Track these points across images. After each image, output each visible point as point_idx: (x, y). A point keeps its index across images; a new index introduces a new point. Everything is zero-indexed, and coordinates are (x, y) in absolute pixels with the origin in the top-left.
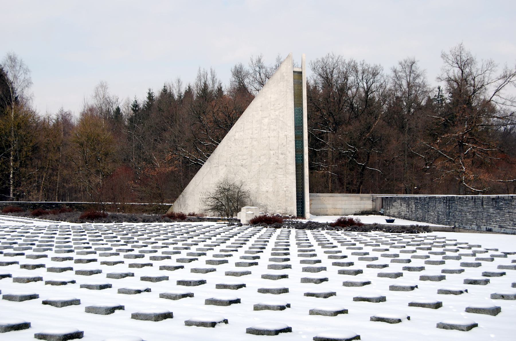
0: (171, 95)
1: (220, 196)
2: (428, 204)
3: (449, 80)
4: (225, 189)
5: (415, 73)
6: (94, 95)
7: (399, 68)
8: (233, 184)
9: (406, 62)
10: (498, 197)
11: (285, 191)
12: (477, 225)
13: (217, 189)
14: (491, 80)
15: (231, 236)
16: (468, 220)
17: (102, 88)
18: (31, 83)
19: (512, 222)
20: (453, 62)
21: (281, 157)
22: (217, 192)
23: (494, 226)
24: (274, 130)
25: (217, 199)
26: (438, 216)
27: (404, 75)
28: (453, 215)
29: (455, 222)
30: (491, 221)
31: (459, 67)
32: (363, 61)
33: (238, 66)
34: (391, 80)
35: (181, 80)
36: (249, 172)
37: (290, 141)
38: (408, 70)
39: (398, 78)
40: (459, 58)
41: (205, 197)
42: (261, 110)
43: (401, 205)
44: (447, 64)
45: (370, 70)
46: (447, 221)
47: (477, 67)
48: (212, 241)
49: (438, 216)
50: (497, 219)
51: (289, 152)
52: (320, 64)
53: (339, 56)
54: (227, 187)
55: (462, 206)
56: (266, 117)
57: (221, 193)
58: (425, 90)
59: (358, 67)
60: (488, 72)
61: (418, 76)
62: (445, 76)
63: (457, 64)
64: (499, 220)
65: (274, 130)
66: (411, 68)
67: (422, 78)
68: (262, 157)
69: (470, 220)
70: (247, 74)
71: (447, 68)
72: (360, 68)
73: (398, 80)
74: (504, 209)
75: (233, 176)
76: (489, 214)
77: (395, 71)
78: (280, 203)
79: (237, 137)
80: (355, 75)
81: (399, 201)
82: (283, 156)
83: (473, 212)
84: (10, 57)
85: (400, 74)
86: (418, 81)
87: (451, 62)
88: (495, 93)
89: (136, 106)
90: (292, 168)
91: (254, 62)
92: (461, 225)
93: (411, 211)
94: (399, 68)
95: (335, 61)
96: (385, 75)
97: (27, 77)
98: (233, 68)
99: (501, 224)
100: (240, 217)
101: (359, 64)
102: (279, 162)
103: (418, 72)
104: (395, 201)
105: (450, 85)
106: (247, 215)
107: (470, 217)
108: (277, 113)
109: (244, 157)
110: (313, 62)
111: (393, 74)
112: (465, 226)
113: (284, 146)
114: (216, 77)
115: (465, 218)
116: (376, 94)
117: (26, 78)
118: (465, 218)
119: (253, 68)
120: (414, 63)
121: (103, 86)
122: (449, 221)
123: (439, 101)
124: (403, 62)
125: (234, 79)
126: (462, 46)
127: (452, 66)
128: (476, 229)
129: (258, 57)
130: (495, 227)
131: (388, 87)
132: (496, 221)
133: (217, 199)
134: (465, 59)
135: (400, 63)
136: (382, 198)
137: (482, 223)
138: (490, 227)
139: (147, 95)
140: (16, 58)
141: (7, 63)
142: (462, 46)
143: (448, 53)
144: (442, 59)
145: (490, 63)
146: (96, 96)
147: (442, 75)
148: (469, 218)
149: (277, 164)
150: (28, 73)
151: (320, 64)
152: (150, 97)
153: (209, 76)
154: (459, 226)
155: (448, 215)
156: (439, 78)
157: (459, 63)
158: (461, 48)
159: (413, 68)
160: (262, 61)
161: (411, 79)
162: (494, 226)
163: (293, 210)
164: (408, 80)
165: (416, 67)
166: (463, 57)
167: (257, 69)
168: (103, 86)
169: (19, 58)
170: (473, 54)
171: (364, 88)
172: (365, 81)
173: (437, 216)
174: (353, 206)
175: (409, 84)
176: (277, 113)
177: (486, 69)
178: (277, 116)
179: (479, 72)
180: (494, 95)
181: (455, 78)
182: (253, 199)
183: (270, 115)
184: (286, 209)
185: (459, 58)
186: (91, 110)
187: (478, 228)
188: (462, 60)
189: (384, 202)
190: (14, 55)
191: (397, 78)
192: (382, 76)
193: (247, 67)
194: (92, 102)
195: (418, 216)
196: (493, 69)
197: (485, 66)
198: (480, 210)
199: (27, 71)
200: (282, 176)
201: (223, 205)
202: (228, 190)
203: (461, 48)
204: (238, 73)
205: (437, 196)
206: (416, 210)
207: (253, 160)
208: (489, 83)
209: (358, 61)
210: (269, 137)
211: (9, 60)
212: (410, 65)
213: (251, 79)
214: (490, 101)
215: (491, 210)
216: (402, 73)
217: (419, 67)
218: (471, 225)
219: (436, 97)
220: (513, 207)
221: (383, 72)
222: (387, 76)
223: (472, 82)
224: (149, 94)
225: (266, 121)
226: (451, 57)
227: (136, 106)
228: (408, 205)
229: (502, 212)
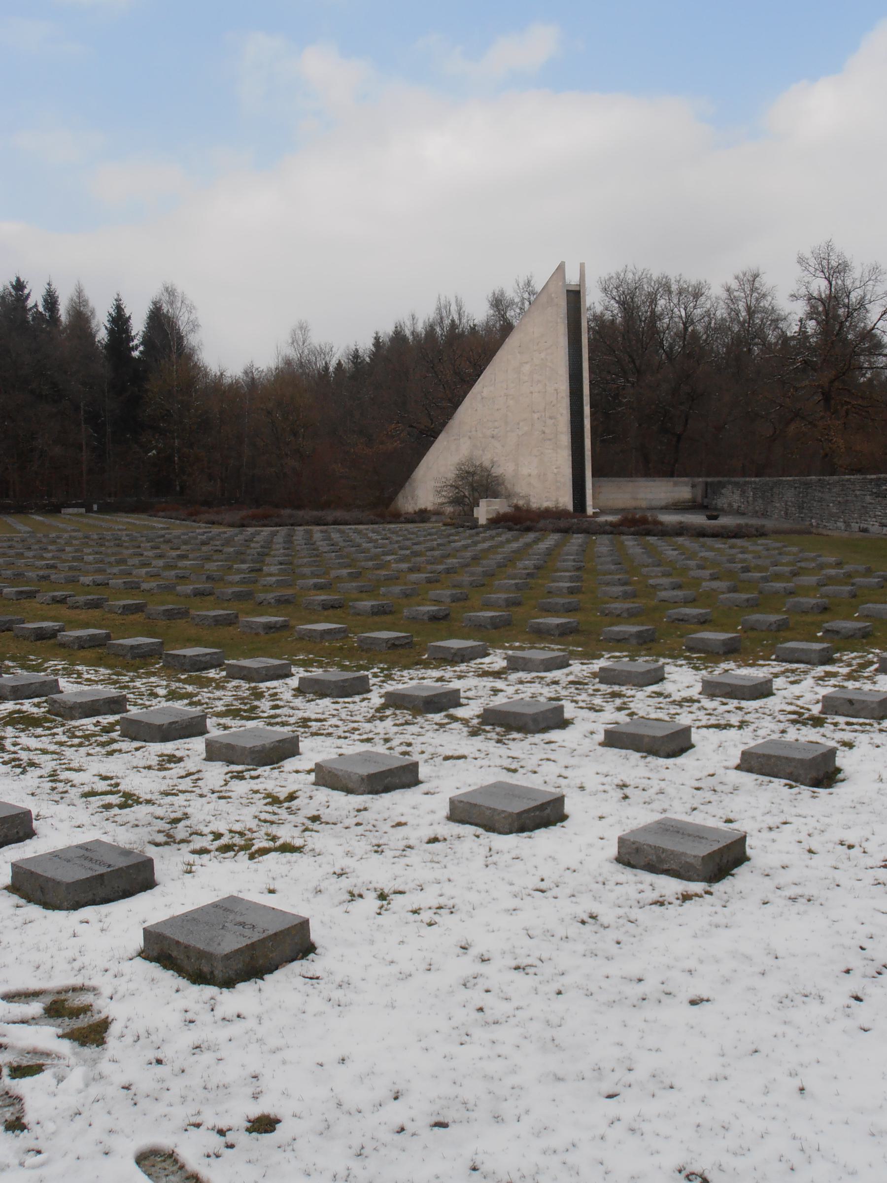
0: (404, 338)
1: (460, 483)
2: (771, 489)
3: (810, 298)
4: (468, 472)
5: (759, 291)
6: (290, 341)
7: (734, 285)
8: (481, 465)
9: (744, 275)
10: (879, 479)
11: (556, 474)
12: (845, 522)
13: (457, 472)
14: (875, 296)
17: (301, 331)
18: (198, 326)
20: (816, 269)
21: (550, 422)
22: (458, 476)
24: (539, 381)
25: (457, 488)
26: (787, 509)
27: (742, 295)
28: (810, 507)
29: (812, 518)
30: (867, 515)
31: (826, 278)
32: (680, 275)
33: (496, 292)
34: (722, 303)
35: (417, 316)
36: (503, 446)
37: (562, 397)
38: (747, 288)
39: (733, 300)
40: (825, 263)
41: (438, 485)
42: (519, 353)
44: (806, 272)
45: (690, 289)
46: (799, 517)
47: (854, 276)
50: (877, 513)
51: (562, 414)
52: (613, 281)
53: (644, 270)
54: (471, 470)
55: (823, 492)
56: (526, 363)
57: (463, 478)
58: (774, 317)
59: (673, 286)
60: (871, 282)
61: (764, 296)
62: (803, 291)
63: (823, 271)
64: (880, 513)
65: (539, 381)
66: (753, 284)
67: (769, 298)
68: (521, 424)
70: (512, 303)
71: (806, 279)
72: (674, 287)
73: (734, 304)
75: (481, 452)
76: (865, 505)
77: (728, 290)
78: (548, 492)
79: (485, 394)
80: (667, 298)
81: (730, 487)
82: (553, 421)
83: (839, 502)
84: (167, 289)
85: (736, 294)
86: (764, 303)
87: (812, 270)
88: (882, 315)
89: (356, 356)
90: (565, 439)
91: (520, 285)
92: (819, 522)
93: (748, 502)
94: (734, 285)
95: (637, 278)
96: (713, 296)
97: (192, 317)
98: (490, 295)
99: (883, 521)
101: (673, 281)
102: (547, 431)
103: (764, 290)
104: (724, 487)
105: (812, 307)
106: (488, 512)
108: (543, 355)
109: (496, 424)
110: (603, 279)
111: (724, 295)
112: (826, 524)
113: (553, 406)
114: (463, 309)
116: (700, 328)
117: (191, 319)
119: (520, 294)
120: (757, 276)
121: (303, 328)
122: (802, 515)
123: (798, 339)
124: (741, 276)
125: (492, 312)
126: (830, 244)
127: (814, 276)
128: (843, 528)
129: (526, 278)
130: (873, 525)
131: (718, 314)
132: (875, 516)
133: (457, 488)
134: (834, 264)
135: (737, 278)
136: (707, 484)
137: (853, 519)
138: (865, 526)
139: (372, 341)
140: (175, 290)
141: (163, 298)
142: (830, 244)
143: (808, 255)
144: (798, 266)
145: (875, 269)
146: (293, 343)
147: (798, 290)
149: (544, 433)
150: (193, 311)
151: (615, 282)
152: (377, 343)
153: (454, 308)
154: (818, 524)
155: (801, 508)
156: (792, 296)
157: (826, 270)
158: (829, 246)
159: (757, 285)
160: (532, 283)
161: (754, 302)
163: (566, 501)
164: (749, 303)
165: (760, 282)
166: (833, 261)
167: (526, 295)
168: (303, 328)
169: (179, 290)
170: (848, 256)
171: (681, 317)
172: (683, 306)
173: (784, 509)
174: (662, 496)
175: (748, 308)
176: (543, 355)
177: (867, 279)
178: (542, 359)
179: (857, 284)
180: (879, 319)
181: (821, 296)
182: (509, 486)
183: (532, 359)
184: (557, 500)
185: (825, 263)
186: (288, 362)
187: (846, 527)
188: (830, 266)
189: (709, 488)
190: (172, 285)
191: (732, 300)
192: (708, 298)
193: (511, 294)
194: (292, 353)
195: (757, 508)
196: (878, 278)
197: (867, 274)
199: (191, 309)
200: (550, 451)
201: (466, 497)
202: (473, 474)
203: (829, 246)
204: (498, 303)
205: (784, 478)
206: (755, 500)
207: (508, 429)
208: (872, 300)
209: (673, 276)
210: (532, 393)
211: (165, 294)
212: (751, 279)
213: (518, 311)
214: (873, 329)
215: (868, 499)
216: (738, 293)
217: (767, 281)
218: (836, 521)
219: (796, 334)
221: (710, 291)
222: (716, 298)
223: (846, 301)
224: (375, 338)
225: (527, 368)
226: (813, 262)
227: (356, 356)
228: (743, 492)
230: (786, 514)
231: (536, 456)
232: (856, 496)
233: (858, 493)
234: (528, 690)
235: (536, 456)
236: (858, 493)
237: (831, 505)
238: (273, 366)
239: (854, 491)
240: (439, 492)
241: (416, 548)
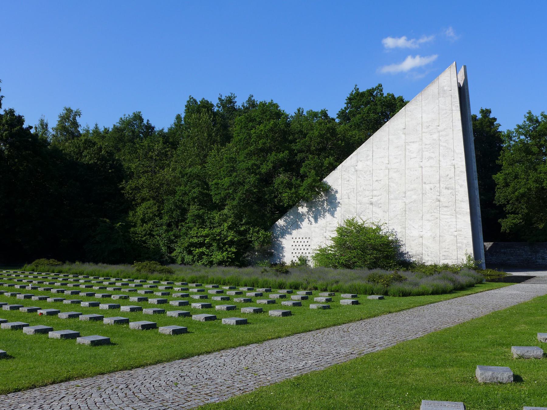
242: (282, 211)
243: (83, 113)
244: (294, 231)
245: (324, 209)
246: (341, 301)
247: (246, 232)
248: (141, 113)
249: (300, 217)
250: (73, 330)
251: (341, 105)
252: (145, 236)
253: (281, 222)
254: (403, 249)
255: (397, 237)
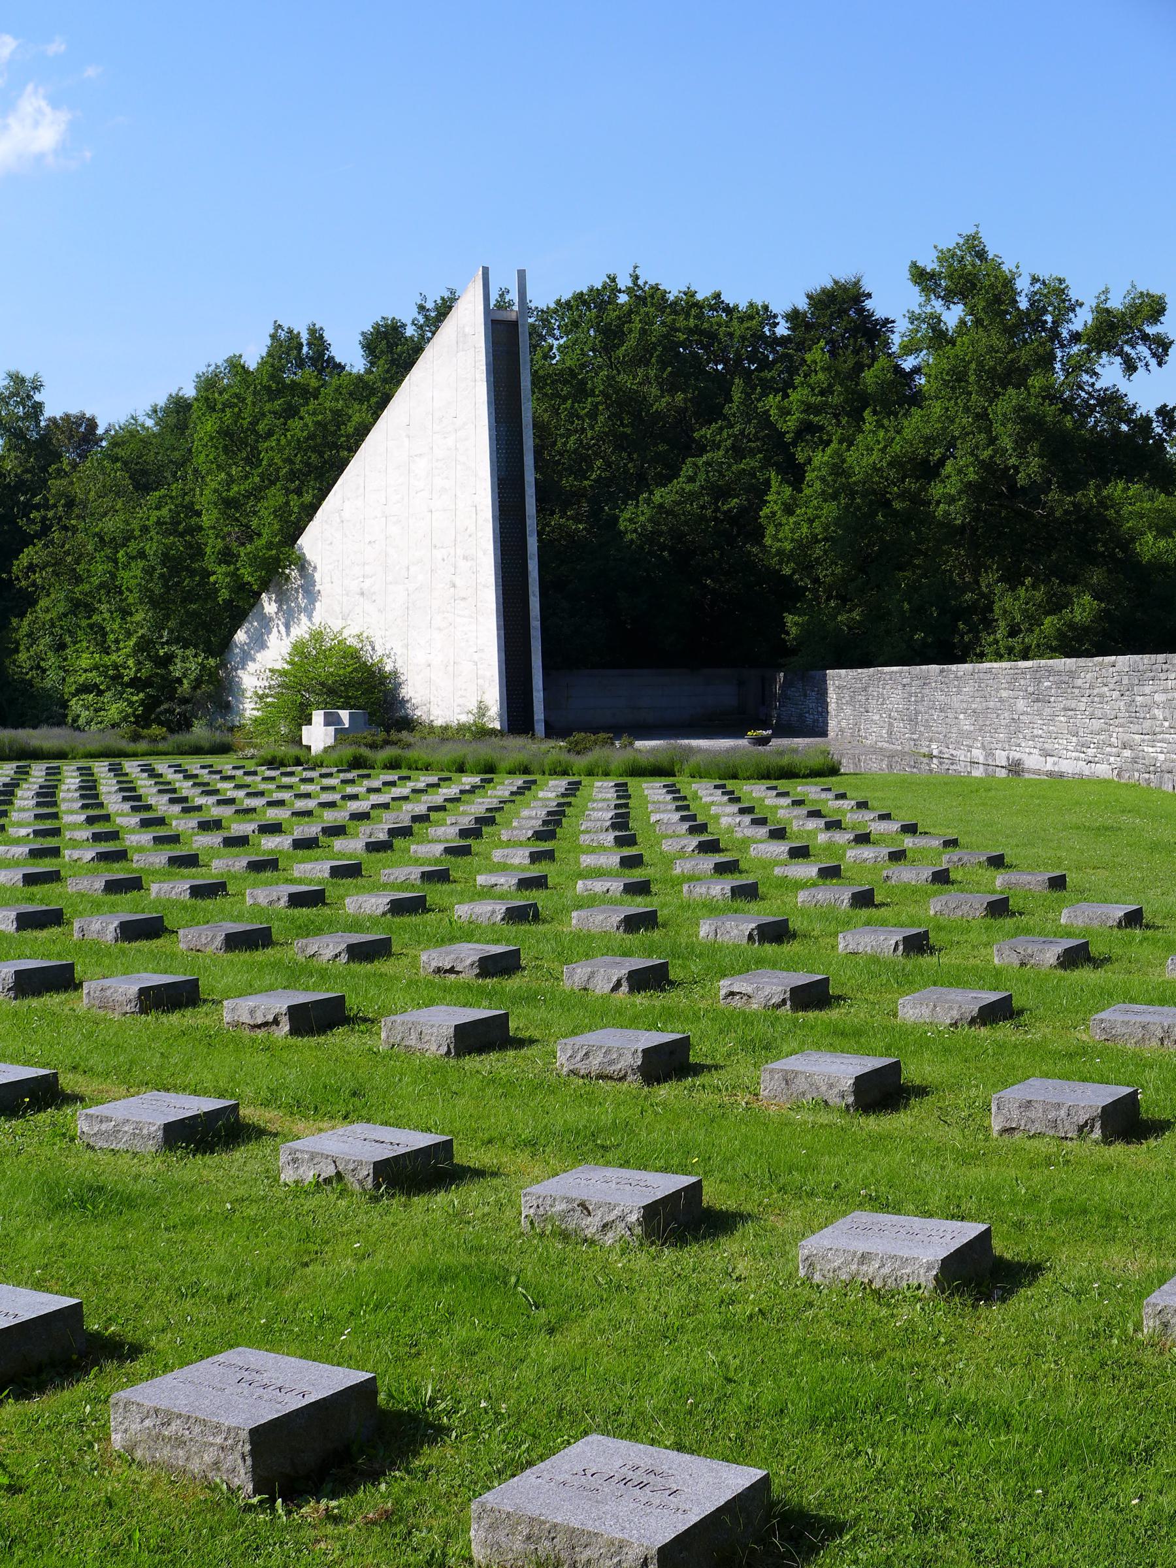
2: (865, 689)
12: (983, 747)
15: (468, 787)
16: (960, 732)
19: (1074, 739)
23: (1027, 750)
26: (891, 725)
41: (258, 684)
43: (805, 696)
46: (910, 739)
48: (197, 814)
49: (891, 725)
50: (1036, 732)
69: (968, 735)
74: (1052, 699)
78: (462, 696)
94: (624, 282)
99: (1046, 746)
100: (309, 739)
102: (458, 583)
107: (967, 725)
112: (954, 752)
115: (954, 730)
118: (954, 730)
122: (915, 737)
130: (1030, 753)
148: (965, 727)
155: (913, 721)
162: (1027, 750)
198: (991, 704)
215: (1021, 705)
220: (1076, 691)
229: (1047, 711)
230: (890, 733)
231: (439, 629)
232: (1001, 700)
233: (1004, 694)
234: (834, 1068)
235: (439, 629)
236: (1004, 694)
237: (962, 716)
238: (122, 422)
239: (997, 690)
240: (261, 697)
241: (350, 790)
242: (238, 617)
243: (45, 380)
244: (258, 655)
245: (298, 606)
246: (582, 837)
247: (169, 659)
248: (930, 263)
249: (266, 622)
250: (658, 1030)
251: (58, 414)
252: (31, 669)
253: (241, 636)
254: (406, 692)
255: (397, 666)
